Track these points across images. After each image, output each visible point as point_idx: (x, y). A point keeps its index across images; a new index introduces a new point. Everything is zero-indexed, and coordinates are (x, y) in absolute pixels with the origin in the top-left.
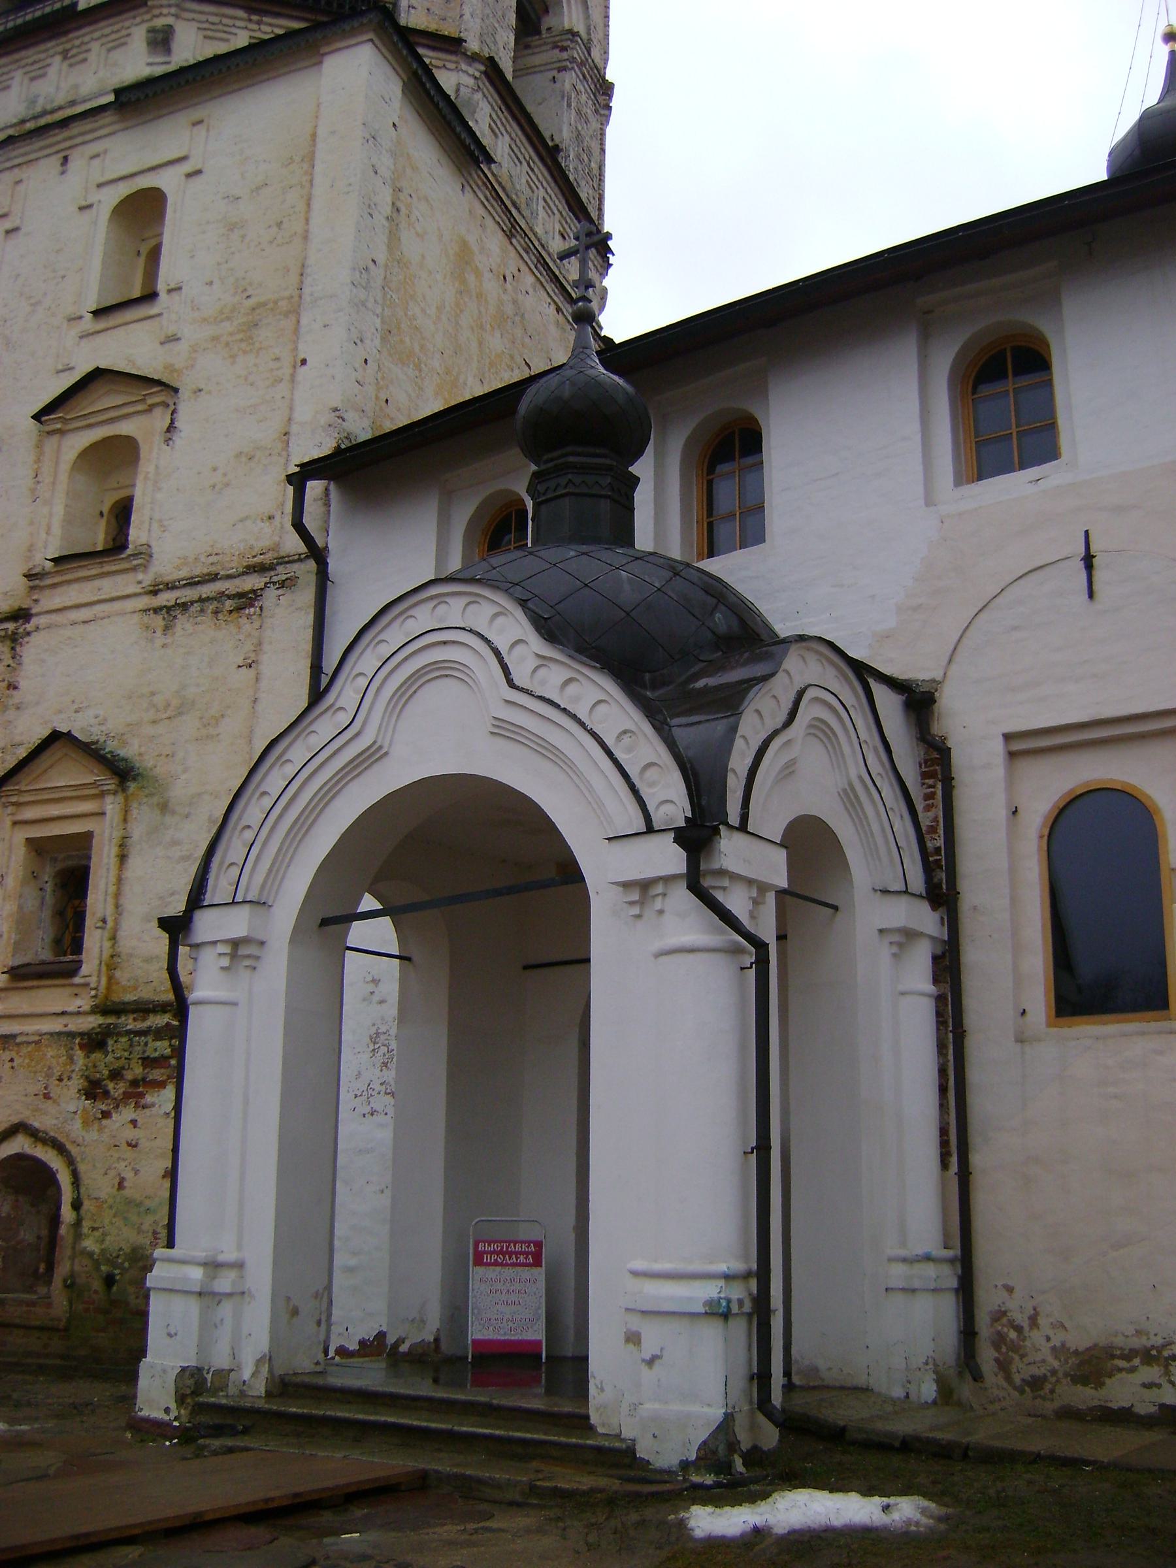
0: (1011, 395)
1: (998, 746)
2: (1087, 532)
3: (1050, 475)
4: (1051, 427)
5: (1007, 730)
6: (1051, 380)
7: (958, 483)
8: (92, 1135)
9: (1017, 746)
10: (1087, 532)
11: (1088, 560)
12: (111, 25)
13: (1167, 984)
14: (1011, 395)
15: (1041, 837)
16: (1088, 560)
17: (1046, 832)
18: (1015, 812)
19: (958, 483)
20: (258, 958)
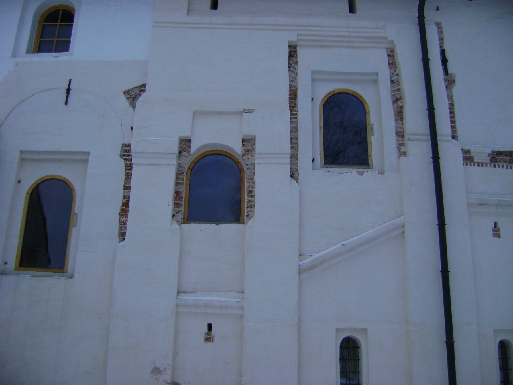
0: (58, 27)
1: (17, 155)
2: (70, 80)
3: (62, 57)
4: (69, 42)
5: (22, 149)
6: (72, 25)
7: (28, 52)
8: (185, 166)
9: (24, 156)
10: (70, 80)
11: (68, 90)
12: (185, 197)
13: (64, 263)
14: (58, 27)
15: (27, 194)
16: (68, 90)
17: (196, 161)
18: (19, 182)
19: (28, 52)
20: (474, 165)
